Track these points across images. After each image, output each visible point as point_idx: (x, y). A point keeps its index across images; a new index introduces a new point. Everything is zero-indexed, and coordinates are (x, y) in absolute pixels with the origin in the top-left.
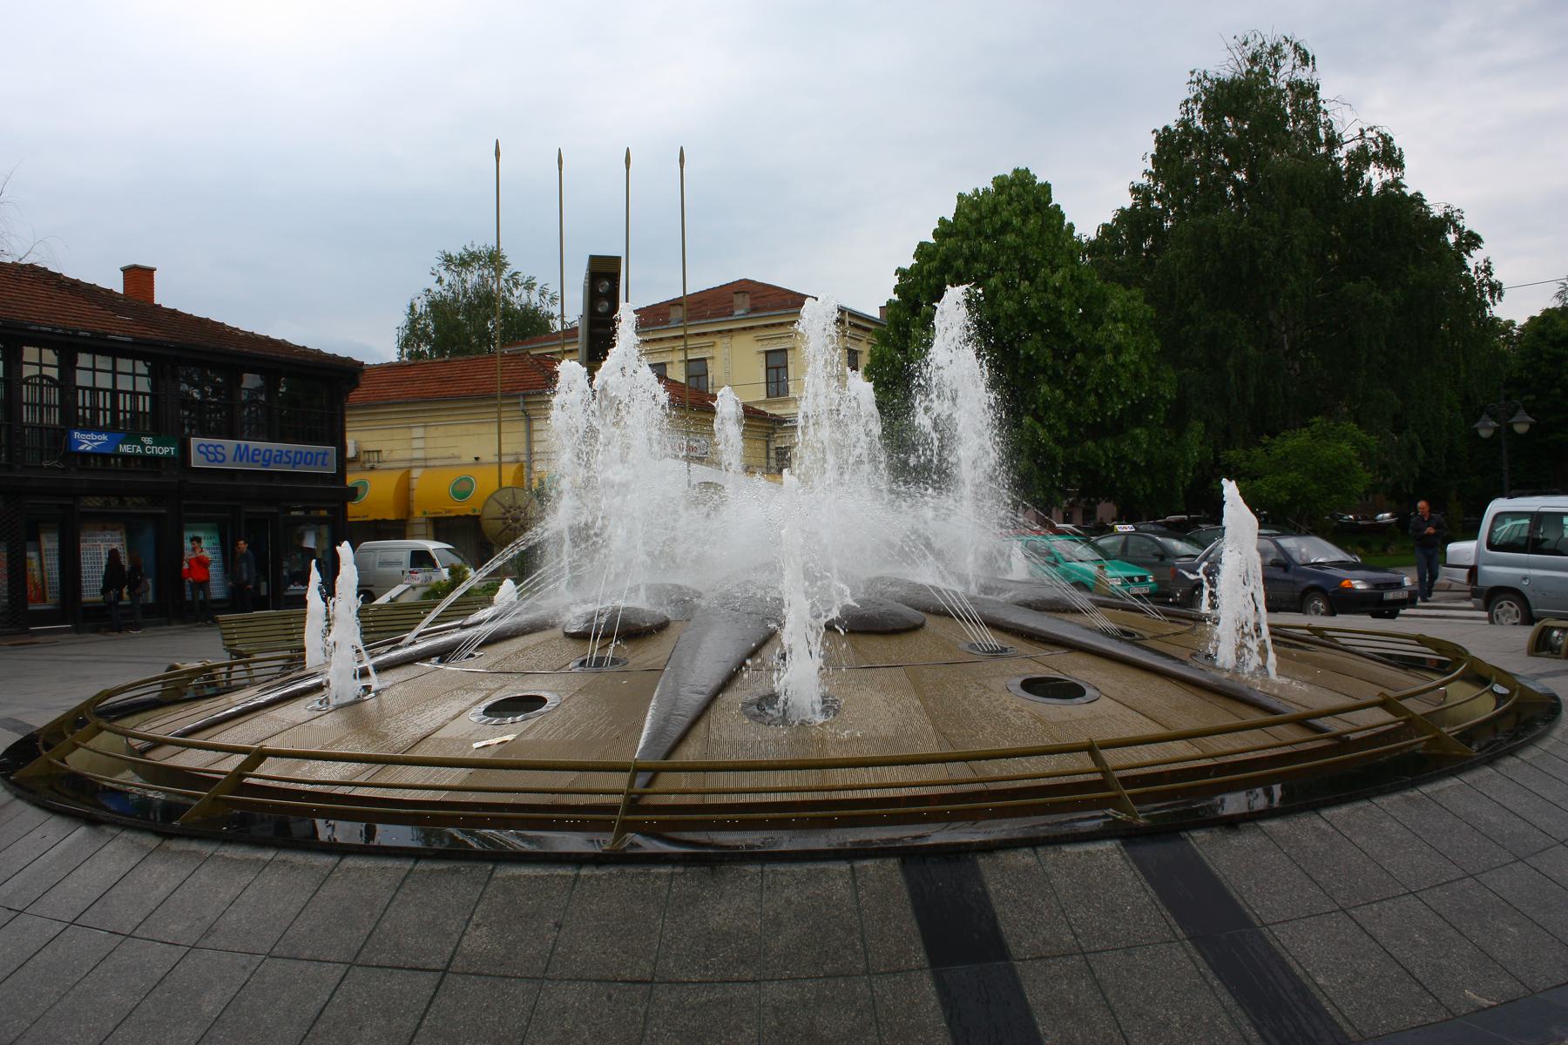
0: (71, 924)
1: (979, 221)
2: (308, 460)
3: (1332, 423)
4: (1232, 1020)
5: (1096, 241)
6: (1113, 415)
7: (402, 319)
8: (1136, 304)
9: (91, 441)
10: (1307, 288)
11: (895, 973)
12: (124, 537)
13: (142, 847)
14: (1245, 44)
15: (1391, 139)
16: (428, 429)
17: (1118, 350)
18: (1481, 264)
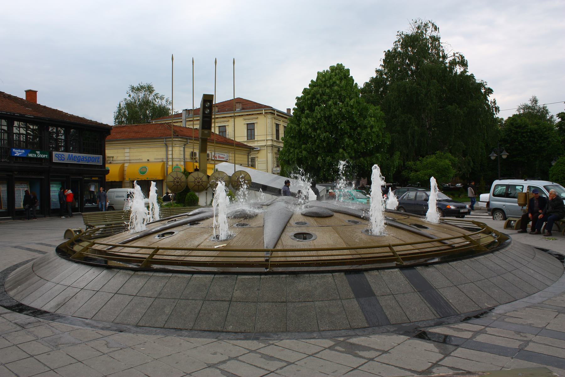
0: (116, 293)
1: (325, 81)
2: (93, 160)
3: (443, 153)
4: (430, 309)
5: (363, 88)
6: (370, 149)
7: (116, 110)
8: (378, 111)
9: (19, 152)
10: (435, 107)
11: (347, 299)
12: (29, 186)
13: (129, 274)
14: (416, 22)
15: (464, 57)
16: (131, 149)
17: (372, 127)
18: (493, 101)
